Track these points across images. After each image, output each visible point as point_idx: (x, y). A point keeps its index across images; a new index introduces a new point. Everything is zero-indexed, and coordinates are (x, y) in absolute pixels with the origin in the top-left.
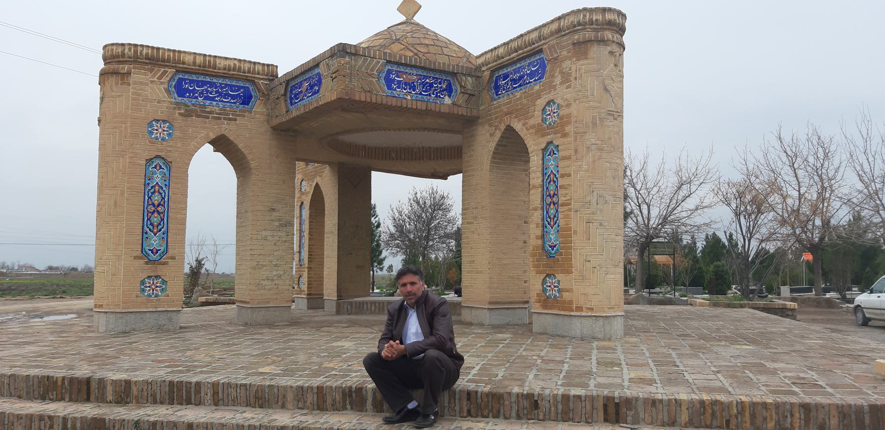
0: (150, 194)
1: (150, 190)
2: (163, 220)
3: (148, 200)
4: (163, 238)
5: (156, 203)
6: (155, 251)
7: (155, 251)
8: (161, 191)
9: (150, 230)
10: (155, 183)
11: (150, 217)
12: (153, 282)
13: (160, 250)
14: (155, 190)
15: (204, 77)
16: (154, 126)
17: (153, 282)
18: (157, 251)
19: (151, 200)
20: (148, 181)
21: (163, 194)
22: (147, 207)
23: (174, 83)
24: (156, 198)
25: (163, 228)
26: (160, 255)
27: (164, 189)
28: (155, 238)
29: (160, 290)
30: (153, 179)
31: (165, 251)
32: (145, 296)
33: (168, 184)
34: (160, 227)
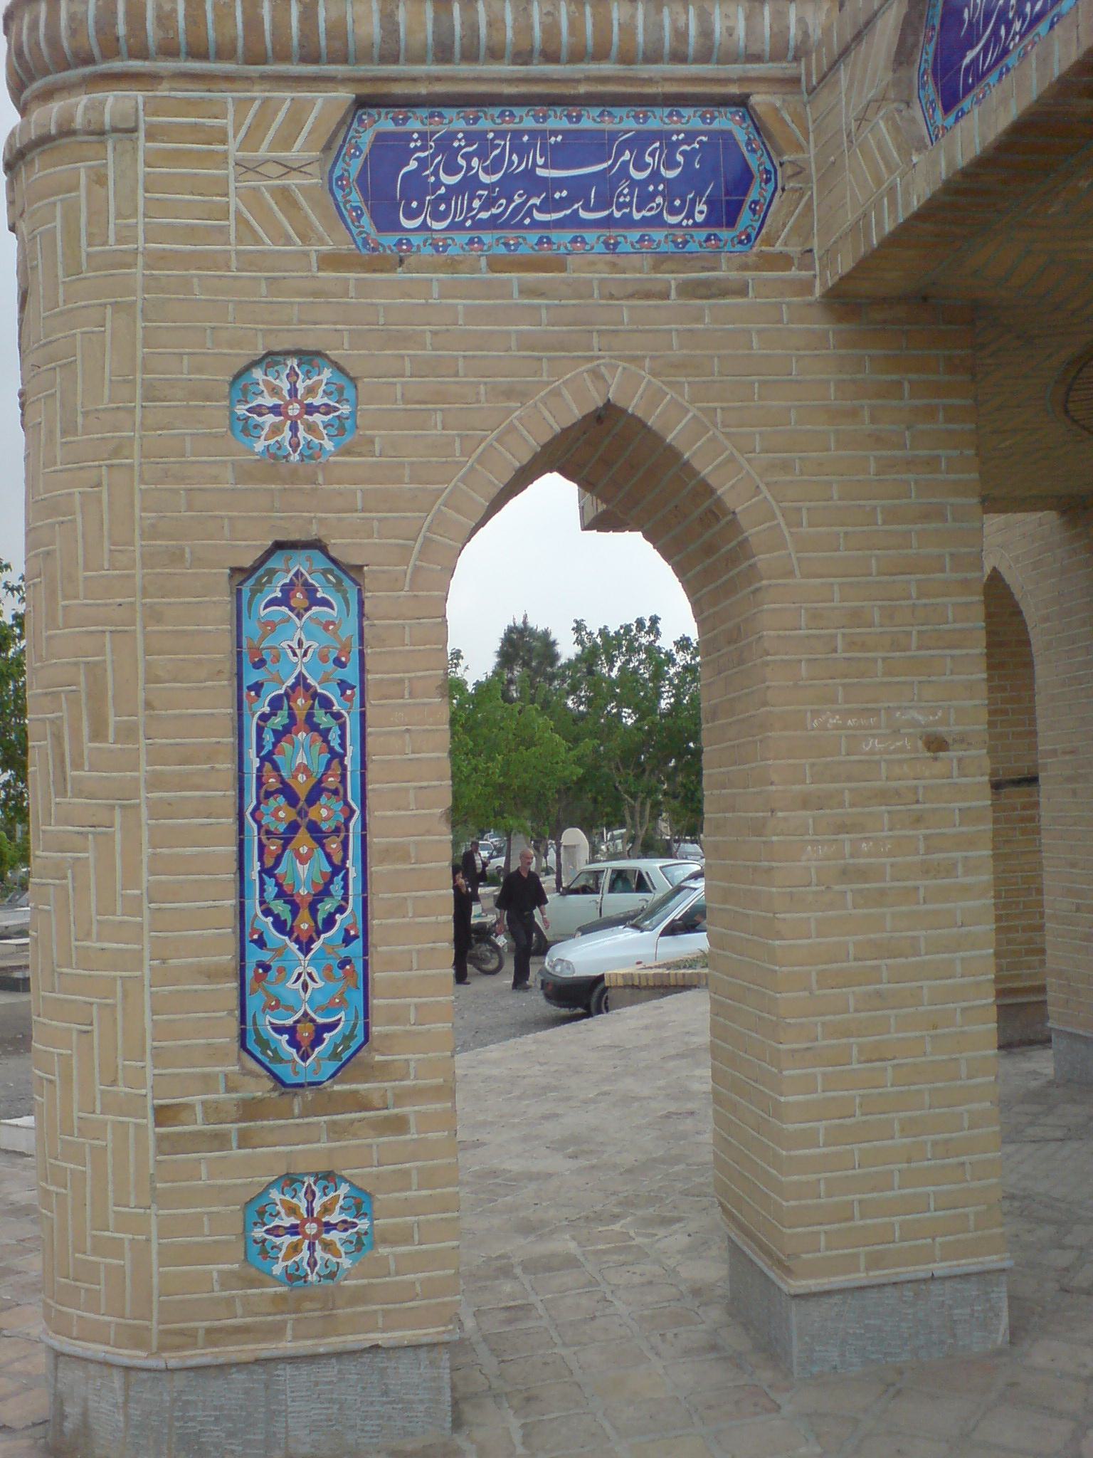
0: (269, 738)
1: (264, 717)
2: (338, 869)
3: (345, 858)
4: (260, 664)
5: (302, 784)
6: (305, 1033)
7: (305, 1033)
8: (323, 719)
9: (280, 925)
10: (316, 946)
11: (278, 860)
12: (294, 385)
13: (331, 1027)
14: (292, 716)
15: (502, 115)
16: (325, 1191)
17: (295, 434)
18: (284, 601)
19: (276, 768)
20: (251, 676)
21: (271, 890)
22: (348, 820)
23: (355, 166)
24: (301, 759)
25: (341, 909)
26: (334, 1055)
27: (336, 708)
28: (304, 964)
29: (345, 1242)
30: (276, 659)
31: (360, 1031)
32: (276, 1280)
33: (251, 948)
34: (279, 721)
